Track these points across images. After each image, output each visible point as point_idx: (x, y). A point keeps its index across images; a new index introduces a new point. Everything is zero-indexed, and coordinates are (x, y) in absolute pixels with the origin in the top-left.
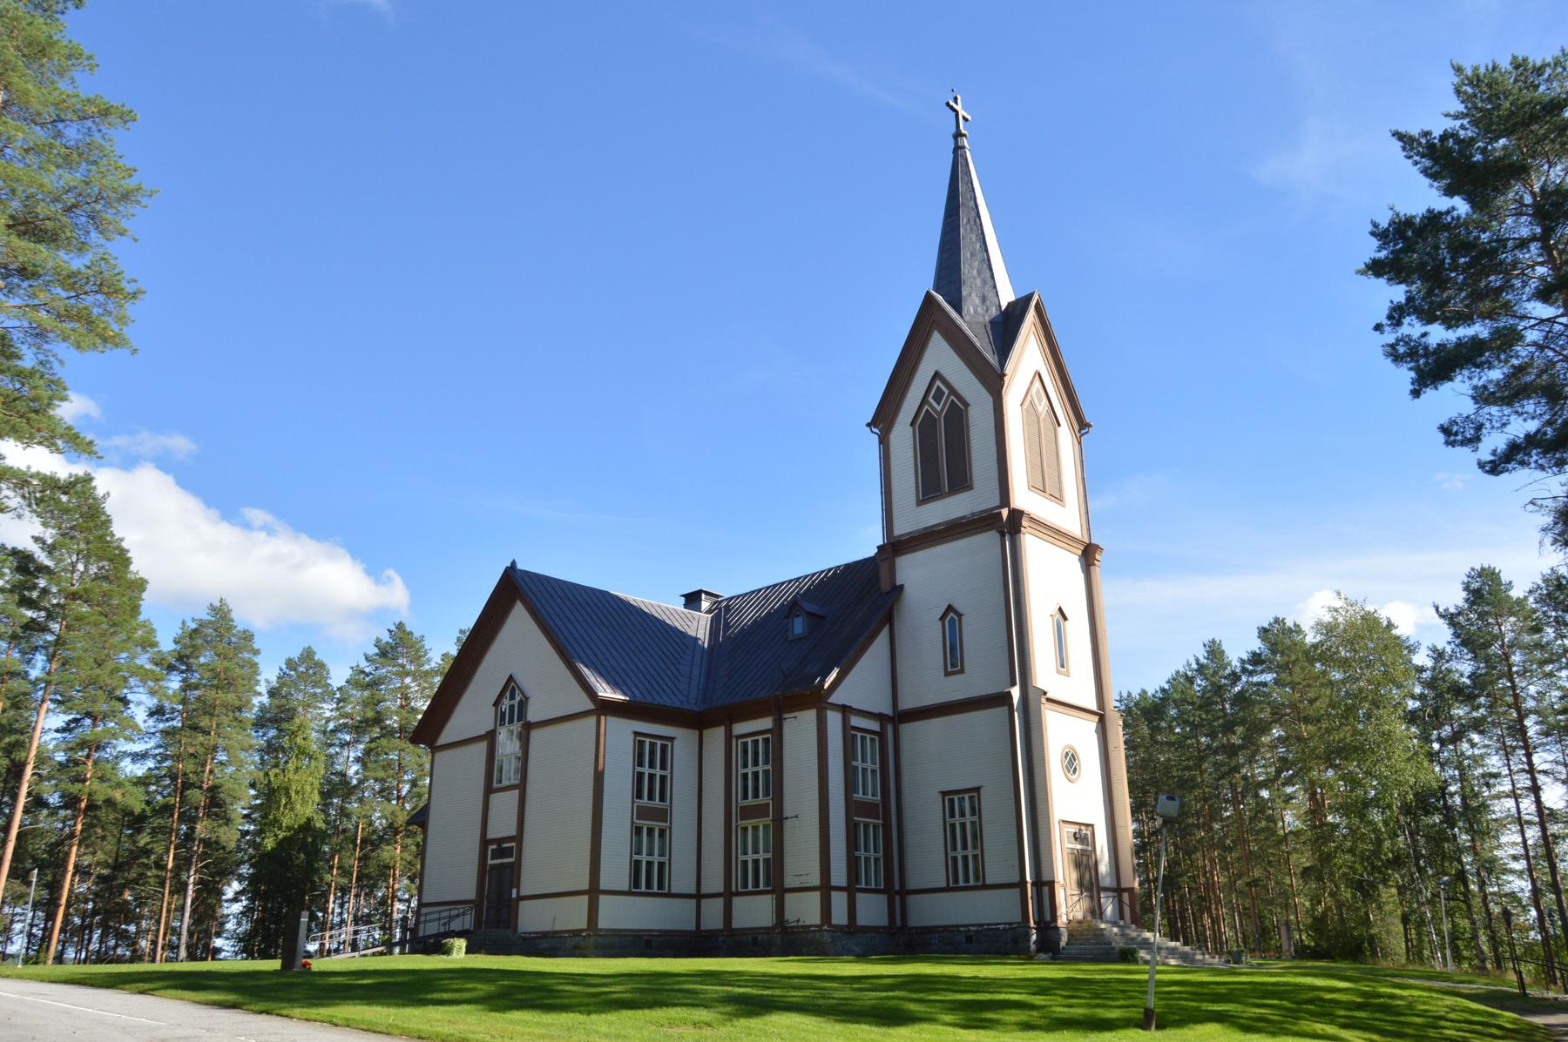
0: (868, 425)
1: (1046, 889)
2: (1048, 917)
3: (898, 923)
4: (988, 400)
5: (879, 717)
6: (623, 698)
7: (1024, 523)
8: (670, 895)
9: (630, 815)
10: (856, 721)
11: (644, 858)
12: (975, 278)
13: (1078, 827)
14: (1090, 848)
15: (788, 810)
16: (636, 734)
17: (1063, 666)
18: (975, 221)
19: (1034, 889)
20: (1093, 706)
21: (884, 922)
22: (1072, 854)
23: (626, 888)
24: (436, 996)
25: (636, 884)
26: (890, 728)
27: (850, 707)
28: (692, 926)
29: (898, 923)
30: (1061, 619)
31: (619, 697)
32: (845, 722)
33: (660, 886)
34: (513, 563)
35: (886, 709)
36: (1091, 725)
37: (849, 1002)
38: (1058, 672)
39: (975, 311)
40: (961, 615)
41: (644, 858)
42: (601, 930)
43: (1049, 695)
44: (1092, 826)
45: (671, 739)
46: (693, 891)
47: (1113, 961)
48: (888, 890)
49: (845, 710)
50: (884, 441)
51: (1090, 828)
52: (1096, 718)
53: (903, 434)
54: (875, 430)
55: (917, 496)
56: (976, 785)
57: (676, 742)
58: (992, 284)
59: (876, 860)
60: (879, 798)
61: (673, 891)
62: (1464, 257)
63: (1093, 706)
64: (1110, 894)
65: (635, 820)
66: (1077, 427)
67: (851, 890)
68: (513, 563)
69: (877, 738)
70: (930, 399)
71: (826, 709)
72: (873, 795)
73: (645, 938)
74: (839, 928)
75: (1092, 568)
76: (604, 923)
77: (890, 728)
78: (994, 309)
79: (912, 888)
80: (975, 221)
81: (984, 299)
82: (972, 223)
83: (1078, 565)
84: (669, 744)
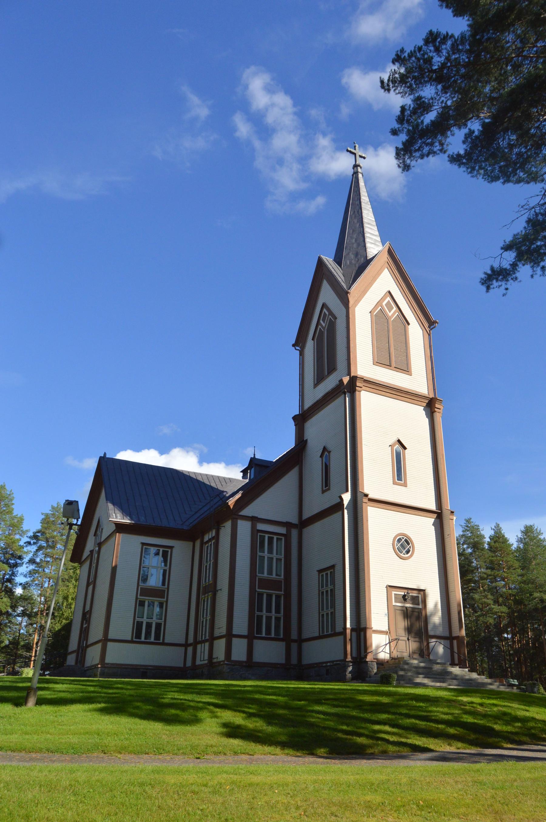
0: (294, 345)
1: (362, 633)
2: (363, 654)
3: (294, 661)
4: (344, 310)
5: (288, 525)
6: (129, 521)
7: (358, 384)
8: (163, 644)
9: (135, 593)
10: (261, 527)
11: (145, 620)
12: (353, 244)
13: (406, 591)
14: (420, 607)
15: (218, 587)
16: (143, 544)
17: (399, 478)
18: (358, 212)
19: (354, 634)
20: (433, 506)
21: (283, 661)
22: (402, 610)
23: (129, 638)
24: (377, 757)
25: (138, 636)
26: (294, 533)
27: (256, 518)
28: (182, 665)
29: (294, 661)
30: (401, 449)
31: (127, 521)
32: (253, 527)
33: (157, 637)
34: (105, 454)
35: (294, 520)
36: (429, 521)
37: (473, 750)
38: (394, 483)
39: (351, 263)
40: (330, 452)
41: (145, 620)
42: (108, 664)
43: (370, 496)
44: (424, 591)
45: (171, 547)
46: (183, 642)
47: (372, 683)
48: (287, 639)
49: (254, 520)
50: (302, 354)
51: (422, 593)
52: (435, 516)
53: (310, 345)
54: (297, 348)
55: (314, 381)
56: (331, 564)
57: (174, 550)
58: (363, 245)
59: (278, 619)
60: (282, 577)
61: (166, 641)
62: (488, 82)
63: (433, 506)
64: (442, 641)
65: (139, 597)
66: (426, 325)
67: (250, 638)
68: (105, 454)
69: (283, 538)
70: (321, 322)
71: (237, 519)
72: (277, 575)
73: (142, 670)
74: (239, 663)
75: (435, 414)
76: (109, 660)
77: (294, 533)
78: (362, 259)
79: (305, 638)
80: (358, 212)
81: (357, 255)
82: (356, 213)
83: (424, 412)
84: (169, 550)
